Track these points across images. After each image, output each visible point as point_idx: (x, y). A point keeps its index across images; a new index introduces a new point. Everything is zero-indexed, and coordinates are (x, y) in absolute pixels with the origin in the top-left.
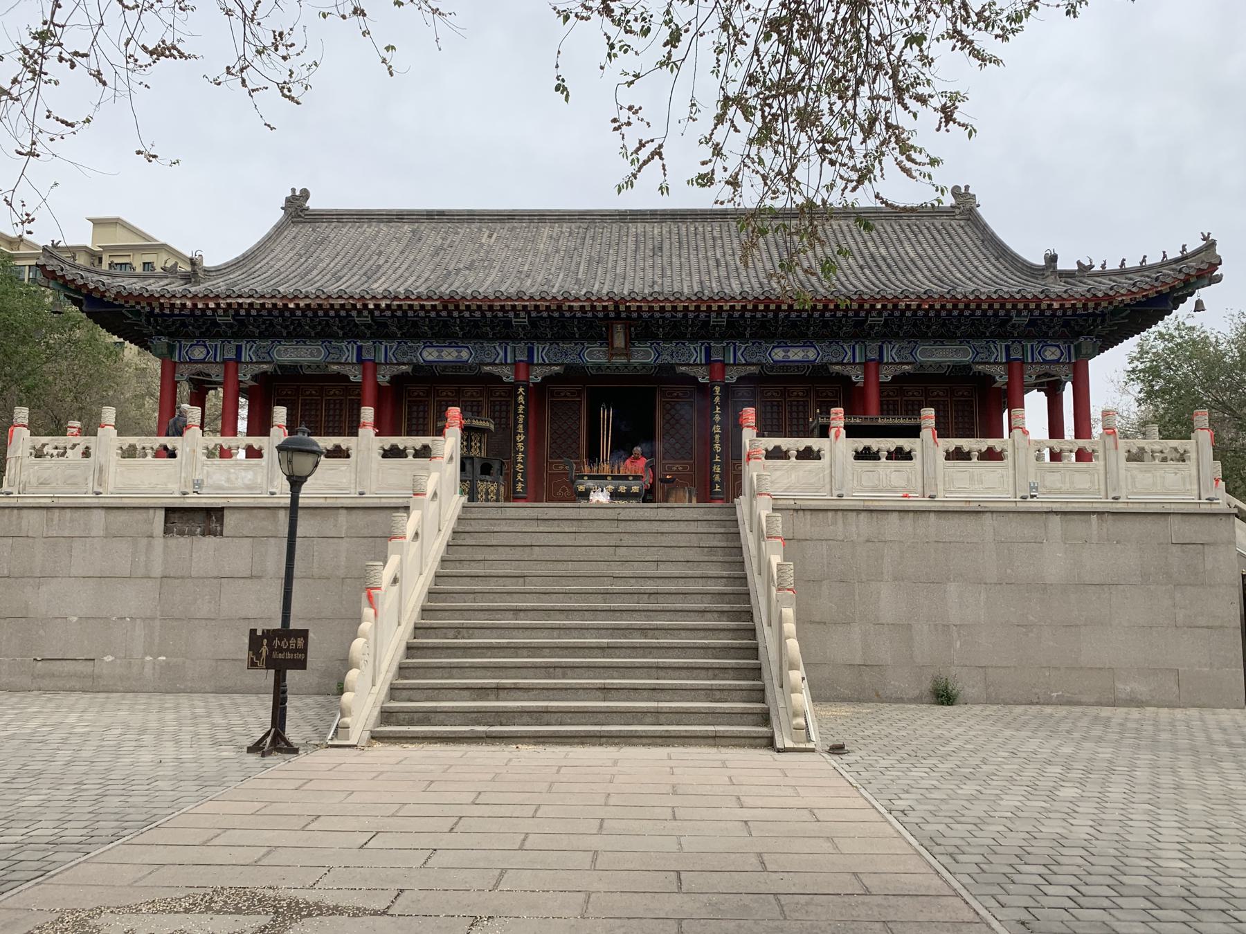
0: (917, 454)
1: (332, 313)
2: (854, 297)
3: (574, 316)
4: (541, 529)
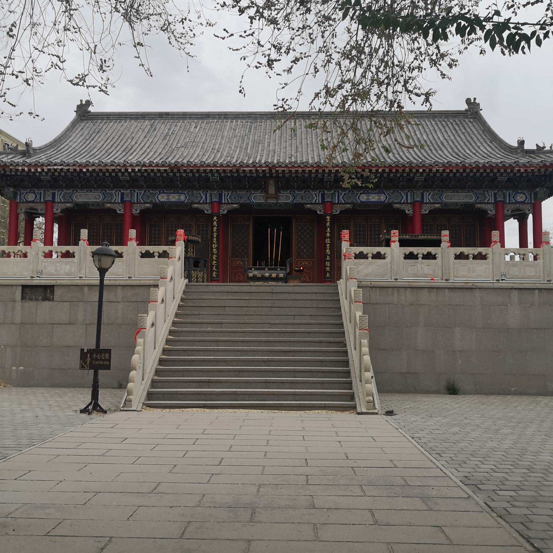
0: (439, 256)
1: (107, 174)
2: (407, 165)
3: (246, 176)
4: (230, 298)
